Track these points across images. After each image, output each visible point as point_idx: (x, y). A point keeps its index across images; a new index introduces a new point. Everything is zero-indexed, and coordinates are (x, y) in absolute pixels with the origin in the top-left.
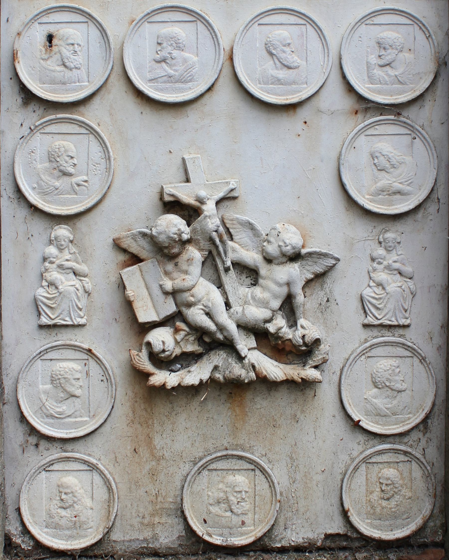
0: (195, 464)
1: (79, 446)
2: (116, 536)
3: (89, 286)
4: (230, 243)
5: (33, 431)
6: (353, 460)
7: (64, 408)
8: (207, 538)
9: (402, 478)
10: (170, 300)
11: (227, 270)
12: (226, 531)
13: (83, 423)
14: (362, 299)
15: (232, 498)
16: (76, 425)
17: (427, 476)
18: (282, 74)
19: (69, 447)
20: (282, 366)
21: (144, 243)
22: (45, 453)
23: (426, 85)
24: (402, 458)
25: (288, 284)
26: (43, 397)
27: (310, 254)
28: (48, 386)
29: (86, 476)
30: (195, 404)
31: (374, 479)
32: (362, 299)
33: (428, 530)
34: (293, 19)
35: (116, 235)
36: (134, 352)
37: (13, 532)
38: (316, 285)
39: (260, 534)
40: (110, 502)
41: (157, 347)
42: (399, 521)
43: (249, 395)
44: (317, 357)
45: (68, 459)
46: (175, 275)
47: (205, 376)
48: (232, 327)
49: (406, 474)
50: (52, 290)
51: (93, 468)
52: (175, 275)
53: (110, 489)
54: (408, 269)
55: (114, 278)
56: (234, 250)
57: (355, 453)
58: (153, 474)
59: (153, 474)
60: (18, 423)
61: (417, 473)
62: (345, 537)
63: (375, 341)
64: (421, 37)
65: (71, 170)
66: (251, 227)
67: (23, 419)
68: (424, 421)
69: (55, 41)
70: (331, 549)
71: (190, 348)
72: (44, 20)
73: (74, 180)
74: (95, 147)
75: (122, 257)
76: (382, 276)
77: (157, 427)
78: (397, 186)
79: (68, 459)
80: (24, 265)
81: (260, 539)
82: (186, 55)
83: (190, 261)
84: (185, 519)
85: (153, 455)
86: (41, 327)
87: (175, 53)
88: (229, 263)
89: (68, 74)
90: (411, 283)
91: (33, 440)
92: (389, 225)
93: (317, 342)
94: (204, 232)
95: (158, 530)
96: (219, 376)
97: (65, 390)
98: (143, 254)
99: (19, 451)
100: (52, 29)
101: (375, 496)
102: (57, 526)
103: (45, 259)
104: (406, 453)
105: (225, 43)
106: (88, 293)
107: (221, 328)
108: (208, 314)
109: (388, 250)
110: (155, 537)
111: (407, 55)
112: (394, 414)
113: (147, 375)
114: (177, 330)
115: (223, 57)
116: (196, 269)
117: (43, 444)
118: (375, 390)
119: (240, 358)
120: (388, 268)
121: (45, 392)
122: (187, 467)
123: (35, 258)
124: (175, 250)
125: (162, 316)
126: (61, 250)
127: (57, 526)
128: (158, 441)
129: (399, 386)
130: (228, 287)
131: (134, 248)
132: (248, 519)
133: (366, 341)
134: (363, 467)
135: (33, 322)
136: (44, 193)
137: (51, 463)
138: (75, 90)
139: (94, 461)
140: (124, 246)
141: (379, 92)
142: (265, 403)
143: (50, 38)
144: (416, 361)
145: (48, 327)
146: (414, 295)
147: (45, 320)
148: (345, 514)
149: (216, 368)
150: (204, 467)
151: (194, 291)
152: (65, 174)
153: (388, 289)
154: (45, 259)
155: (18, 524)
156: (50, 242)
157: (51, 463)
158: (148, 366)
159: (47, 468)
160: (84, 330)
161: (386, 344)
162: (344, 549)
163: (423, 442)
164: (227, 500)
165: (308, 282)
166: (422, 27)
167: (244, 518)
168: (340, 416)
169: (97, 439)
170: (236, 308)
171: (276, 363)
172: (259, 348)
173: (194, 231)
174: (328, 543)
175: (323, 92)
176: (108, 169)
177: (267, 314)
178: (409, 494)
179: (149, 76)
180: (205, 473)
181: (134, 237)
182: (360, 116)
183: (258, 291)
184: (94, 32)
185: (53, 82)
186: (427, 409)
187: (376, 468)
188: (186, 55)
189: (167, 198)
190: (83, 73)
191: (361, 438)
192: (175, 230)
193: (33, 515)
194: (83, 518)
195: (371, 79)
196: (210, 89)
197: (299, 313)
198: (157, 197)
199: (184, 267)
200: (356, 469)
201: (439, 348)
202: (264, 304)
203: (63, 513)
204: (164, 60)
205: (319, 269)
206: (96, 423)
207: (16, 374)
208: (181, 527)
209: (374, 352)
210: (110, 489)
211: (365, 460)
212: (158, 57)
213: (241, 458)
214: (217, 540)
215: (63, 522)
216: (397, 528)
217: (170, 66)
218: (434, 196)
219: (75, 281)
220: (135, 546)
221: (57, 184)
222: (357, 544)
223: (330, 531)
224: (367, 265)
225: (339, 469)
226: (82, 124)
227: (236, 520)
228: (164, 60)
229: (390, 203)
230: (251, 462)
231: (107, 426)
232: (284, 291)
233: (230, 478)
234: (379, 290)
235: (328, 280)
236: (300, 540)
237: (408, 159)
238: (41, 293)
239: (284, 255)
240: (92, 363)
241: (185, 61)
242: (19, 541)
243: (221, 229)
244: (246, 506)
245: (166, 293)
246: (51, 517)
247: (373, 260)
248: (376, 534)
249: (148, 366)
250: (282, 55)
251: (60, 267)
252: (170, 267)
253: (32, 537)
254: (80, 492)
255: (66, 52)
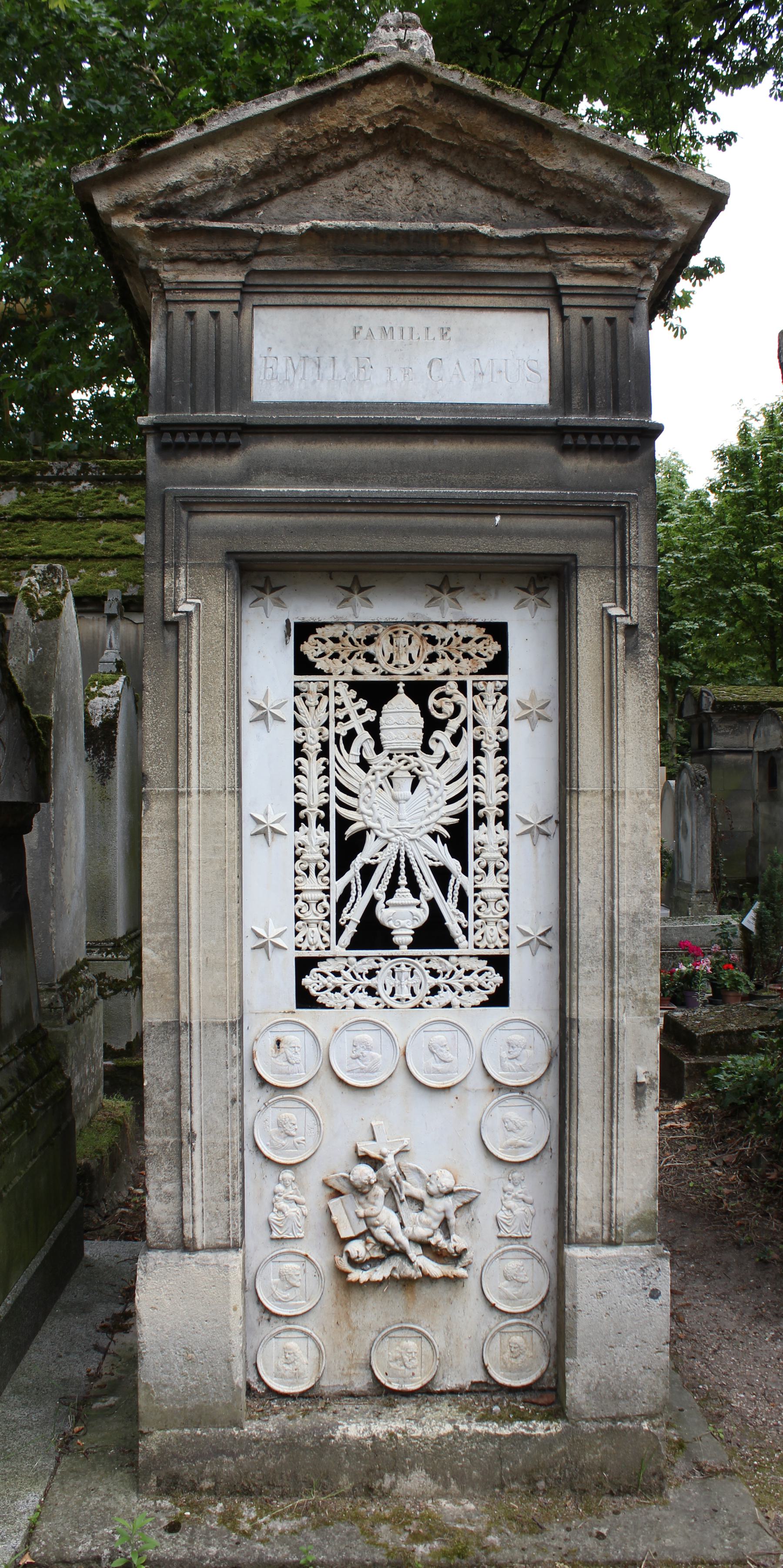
0: (380, 1333)
1: (297, 1320)
2: (324, 1383)
3: (306, 1211)
4: (404, 1182)
5: (266, 1310)
6: (491, 1330)
7: (288, 1294)
8: (388, 1385)
9: (526, 1343)
10: (363, 1223)
11: (402, 1202)
12: (401, 1380)
13: (302, 1305)
14: (497, 1219)
15: (405, 1357)
16: (296, 1306)
17: (544, 1342)
18: (440, 1066)
19: (291, 1321)
20: (440, 1266)
21: (344, 1183)
22: (275, 1325)
23: (542, 1072)
24: (526, 1328)
25: (444, 1212)
26: (274, 1287)
27: (460, 1191)
28: (278, 1280)
29: (304, 1342)
30: (380, 1291)
31: (506, 1343)
32: (497, 1219)
33: (545, 1380)
34: (448, 1027)
35: (325, 1177)
36: (337, 1258)
37: (252, 1380)
38: (465, 1210)
39: (425, 1382)
40: (320, 1360)
41: (354, 1255)
42: (524, 1373)
43: (417, 1285)
44: (465, 1260)
45: (291, 1330)
46: (366, 1205)
47: (387, 1274)
48: (405, 1242)
49: (529, 1340)
50: (280, 1215)
51: (308, 1336)
52: (366, 1205)
53: (320, 1351)
54: (529, 1198)
55: (323, 1206)
56: (407, 1187)
57: (492, 1325)
58: (350, 1340)
59: (350, 1340)
60: (255, 1305)
61: (537, 1339)
62: (486, 1383)
63: (506, 1248)
64: (538, 1038)
65: (293, 1133)
66: (419, 1172)
67: (259, 1301)
68: (542, 1303)
69: (281, 1045)
70: (476, 1392)
71: (376, 1255)
72: (274, 1029)
73: (296, 1139)
74: (310, 1117)
75: (328, 1191)
76: (511, 1203)
77: (353, 1307)
78: (521, 1142)
79: (291, 1330)
80: (261, 1196)
81: (426, 1385)
82: (373, 1053)
83: (376, 1196)
84: (373, 1371)
85: (350, 1326)
86: (272, 1239)
87: (366, 1053)
88: (403, 1197)
89: (291, 1067)
90: (531, 1207)
91: (266, 1316)
92: (517, 1168)
93: (465, 1250)
94: (386, 1176)
95: (353, 1379)
96: (396, 1274)
97: (289, 1283)
98: (343, 1190)
99: (256, 1324)
100: (279, 1036)
101: (507, 1355)
102: (283, 1376)
103: (275, 1194)
104: (528, 1325)
105: (400, 1044)
106: (305, 1216)
107: (398, 1243)
108: (389, 1233)
109: (515, 1185)
110: (351, 1384)
111: (529, 1052)
112: (520, 1298)
113: (346, 1274)
114: (367, 1243)
115: (399, 1053)
116: (380, 1201)
117: (273, 1319)
118: (506, 1282)
119: (411, 1262)
120: (515, 1197)
121: (275, 1284)
122: (374, 1335)
123: (268, 1193)
124: (366, 1190)
125: (357, 1233)
126: (286, 1186)
127: (283, 1376)
128: (354, 1317)
129: (522, 1279)
130: (403, 1213)
131: (338, 1187)
132: (417, 1371)
133: (500, 1247)
134: (498, 1335)
135: (266, 1235)
136: (274, 1149)
137: (279, 1333)
138: (296, 1078)
139: (309, 1331)
140: (331, 1184)
141: (508, 1077)
142: (428, 1291)
143: (278, 1042)
144: (535, 1261)
145: (277, 1239)
146: (533, 1216)
147: (275, 1235)
148: (485, 1368)
149: (394, 1269)
150: (386, 1335)
151: (379, 1217)
152: (289, 1135)
153: (515, 1212)
154: (275, 1194)
155: (255, 1375)
156: (279, 1182)
157: (279, 1333)
158: (346, 1267)
159: (276, 1336)
160: (302, 1242)
161: (513, 1250)
162: (485, 1392)
163: (541, 1317)
164: (402, 1358)
165: (459, 1209)
166: (539, 1031)
167: (415, 1371)
168: (481, 1299)
169: (311, 1316)
170: (408, 1228)
171: (436, 1264)
172: (424, 1254)
173: (379, 1175)
174: (474, 1388)
175: (470, 1078)
176: (319, 1132)
177: (430, 1232)
178: (531, 1354)
179: (347, 1068)
180: (387, 1339)
181: (337, 1179)
182: (495, 1093)
183: (423, 1216)
184: (309, 1038)
185: (280, 1073)
186: (543, 1295)
187: (507, 1336)
188: (373, 1053)
189: (360, 1154)
190: (301, 1066)
191: (496, 1314)
192: (366, 1177)
193: (266, 1369)
194: (301, 1371)
195: (503, 1068)
196: (390, 1076)
197: (452, 1230)
198: (353, 1150)
199: (372, 1200)
200: (493, 1336)
201: (552, 1252)
202: (428, 1225)
203: (287, 1367)
204: (358, 1057)
205: (466, 1200)
206: (75, 734)
207: (254, 1271)
208: (370, 1376)
209: (505, 1256)
210: (320, 1351)
211: (499, 1331)
212: (354, 1055)
213: (411, 1329)
214: (395, 1386)
215: (287, 1374)
216: (522, 1377)
217: (362, 1061)
218: (549, 1147)
219: (296, 1208)
220: (337, 1390)
221: (284, 1142)
222: (494, 1389)
223: (475, 1380)
224: (501, 1195)
225: (481, 1336)
226: (301, 1102)
227: (408, 1372)
228: (358, 1057)
229: (516, 1154)
230: (419, 1332)
231: (318, 1307)
232: (442, 1216)
233: (405, 1343)
234: (509, 1213)
235: (473, 1207)
236: (454, 1386)
237: (529, 1123)
238: (273, 1217)
239: (441, 1192)
240: (308, 1264)
241: (372, 1057)
242: (256, 1387)
243: (398, 1174)
244: (415, 1362)
245: (360, 1218)
246: (278, 1370)
247: (504, 1192)
248: (507, 1382)
249: (346, 1267)
250: (440, 1053)
251: (286, 1198)
252: (362, 1200)
253: (265, 1384)
254: (299, 1352)
255: (290, 1052)
